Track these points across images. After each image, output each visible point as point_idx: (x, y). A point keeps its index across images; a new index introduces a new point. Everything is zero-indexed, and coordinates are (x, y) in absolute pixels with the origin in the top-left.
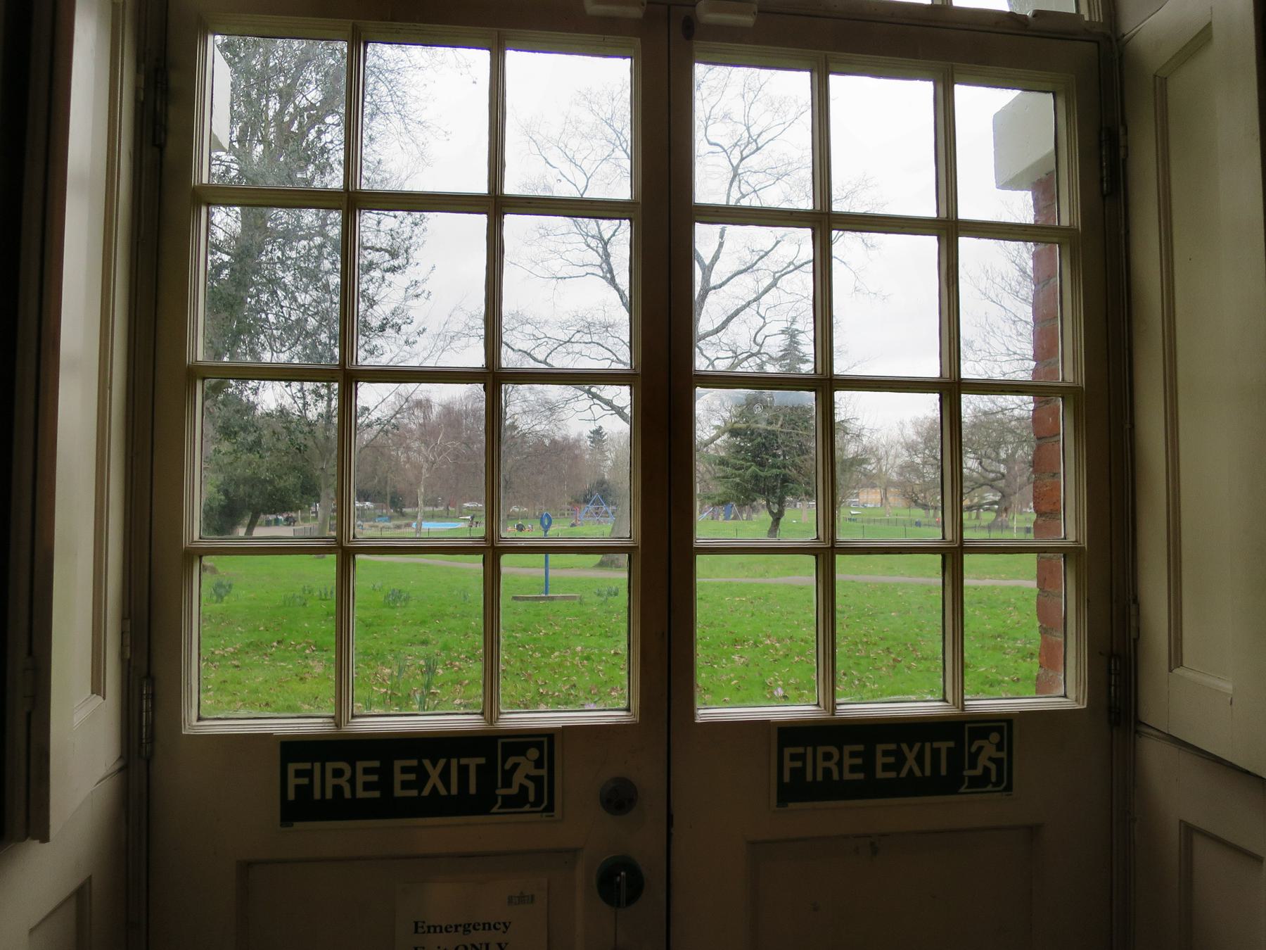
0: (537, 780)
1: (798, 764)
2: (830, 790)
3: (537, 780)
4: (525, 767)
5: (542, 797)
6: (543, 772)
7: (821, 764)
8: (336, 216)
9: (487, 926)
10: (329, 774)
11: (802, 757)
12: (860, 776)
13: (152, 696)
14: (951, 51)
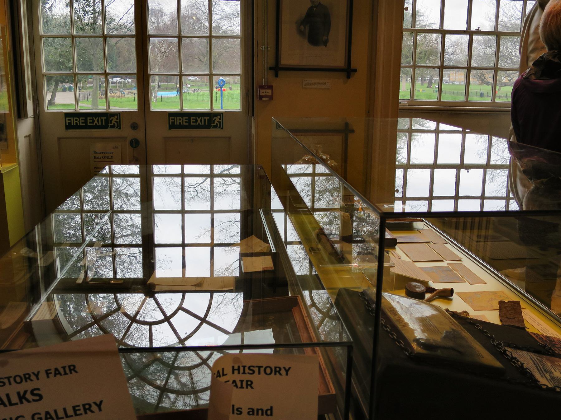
2: (180, 127)
3: (117, 122)
5: (118, 126)
7: (178, 121)
8: (440, 36)
9: (109, 153)
11: (174, 119)
13: (38, 104)
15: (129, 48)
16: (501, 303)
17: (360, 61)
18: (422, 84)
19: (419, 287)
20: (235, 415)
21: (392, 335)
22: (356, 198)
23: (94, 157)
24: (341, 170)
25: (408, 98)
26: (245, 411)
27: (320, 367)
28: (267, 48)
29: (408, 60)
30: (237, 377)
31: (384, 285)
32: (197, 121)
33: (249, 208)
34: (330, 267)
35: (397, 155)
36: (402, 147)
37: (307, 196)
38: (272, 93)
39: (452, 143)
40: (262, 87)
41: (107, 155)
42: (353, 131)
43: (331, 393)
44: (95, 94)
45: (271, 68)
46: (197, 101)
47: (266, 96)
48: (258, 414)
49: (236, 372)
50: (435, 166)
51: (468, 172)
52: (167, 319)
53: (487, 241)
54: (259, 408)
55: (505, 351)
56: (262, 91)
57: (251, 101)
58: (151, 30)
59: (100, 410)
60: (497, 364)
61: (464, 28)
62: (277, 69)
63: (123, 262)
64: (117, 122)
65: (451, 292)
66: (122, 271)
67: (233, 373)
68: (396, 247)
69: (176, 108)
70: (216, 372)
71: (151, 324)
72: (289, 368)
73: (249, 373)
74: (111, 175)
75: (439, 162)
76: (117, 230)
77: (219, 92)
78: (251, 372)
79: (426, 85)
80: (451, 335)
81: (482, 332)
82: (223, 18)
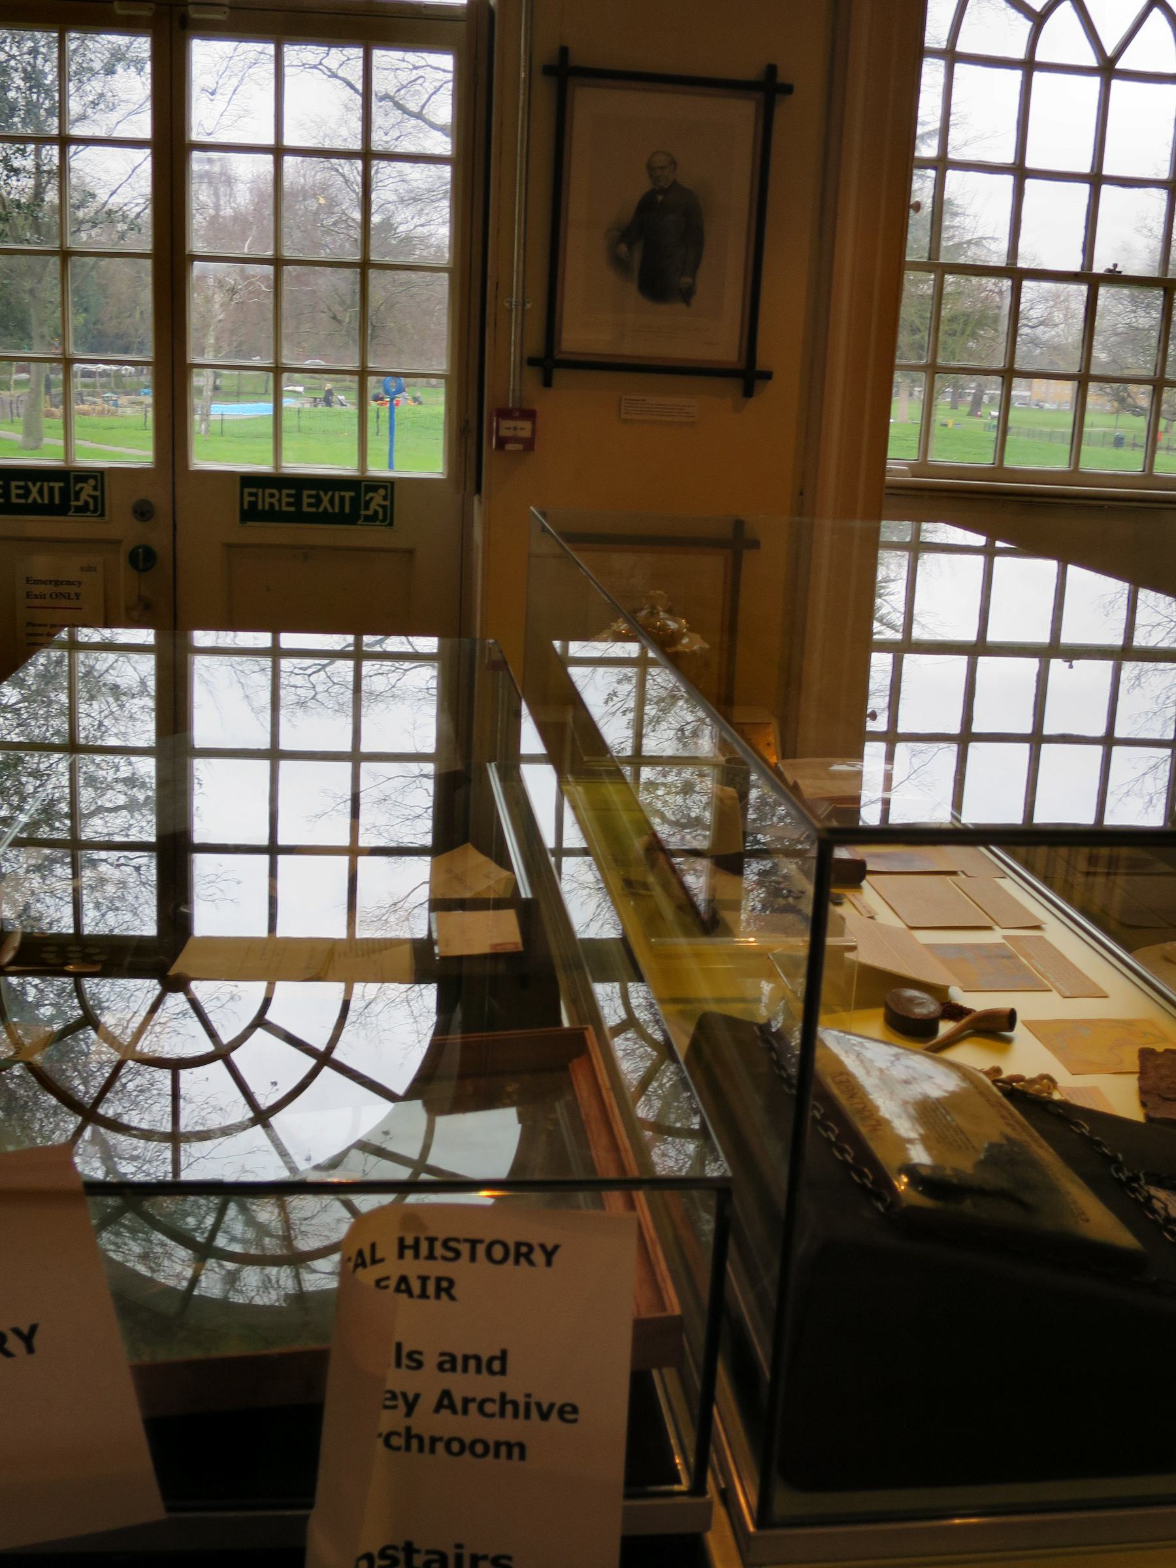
0: (384, 507)
1: (253, 499)
2: (273, 515)
3: (95, 498)
4: (87, 489)
5: (97, 507)
6: (98, 493)
9: (69, 583)
10: (246, 495)
11: (255, 495)
12: (292, 509)
14: (417, 30)
15: (136, 286)
16: (1146, 1055)
17: (780, 349)
18: (954, 406)
19: (921, 1004)
20: (404, 1369)
21: (842, 1151)
22: (753, 777)
23: (28, 595)
24: (717, 688)
25: (913, 455)
26: (431, 1361)
27: (640, 1226)
28: (524, 304)
29: (917, 337)
30: (413, 1268)
31: (826, 993)
32: (319, 501)
33: (459, 766)
34: (682, 943)
35: (878, 601)
36: (892, 576)
37: (624, 713)
38: (534, 431)
39: (1026, 588)
40: (504, 414)
41: (64, 589)
42: (755, 544)
43: (669, 1313)
44: (34, 405)
45: (532, 362)
46: (322, 448)
47: (517, 440)
48: (465, 1369)
49: (409, 1253)
50: (978, 649)
51: (1071, 667)
52: (222, 1053)
53: (1116, 874)
54: (471, 1352)
55: (1150, 1198)
56: (505, 424)
57: (472, 451)
58: (197, 244)
59: (30, 1350)
60: (1125, 1239)
61: (1076, 267)
62: (548, 363)
63: (102, 881)
64: (95, 498)
65: (1009, 1019)
66: (97, 906)
67: (401, 1256)
68: (864, 883)
69: (263, 465)
70: (354, 1255)
71: (176, 1065)
72: (556, 1248)
73: (444, 1258)
74: (74, 646)
75: (992, 637)
76: (86, 795)
77: (385, 412)
78: (451, 1255)
79: (964, 409)
80: (1002, 1157)
81: (1089, 1141)
82: (402, 200)
